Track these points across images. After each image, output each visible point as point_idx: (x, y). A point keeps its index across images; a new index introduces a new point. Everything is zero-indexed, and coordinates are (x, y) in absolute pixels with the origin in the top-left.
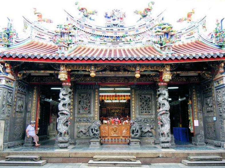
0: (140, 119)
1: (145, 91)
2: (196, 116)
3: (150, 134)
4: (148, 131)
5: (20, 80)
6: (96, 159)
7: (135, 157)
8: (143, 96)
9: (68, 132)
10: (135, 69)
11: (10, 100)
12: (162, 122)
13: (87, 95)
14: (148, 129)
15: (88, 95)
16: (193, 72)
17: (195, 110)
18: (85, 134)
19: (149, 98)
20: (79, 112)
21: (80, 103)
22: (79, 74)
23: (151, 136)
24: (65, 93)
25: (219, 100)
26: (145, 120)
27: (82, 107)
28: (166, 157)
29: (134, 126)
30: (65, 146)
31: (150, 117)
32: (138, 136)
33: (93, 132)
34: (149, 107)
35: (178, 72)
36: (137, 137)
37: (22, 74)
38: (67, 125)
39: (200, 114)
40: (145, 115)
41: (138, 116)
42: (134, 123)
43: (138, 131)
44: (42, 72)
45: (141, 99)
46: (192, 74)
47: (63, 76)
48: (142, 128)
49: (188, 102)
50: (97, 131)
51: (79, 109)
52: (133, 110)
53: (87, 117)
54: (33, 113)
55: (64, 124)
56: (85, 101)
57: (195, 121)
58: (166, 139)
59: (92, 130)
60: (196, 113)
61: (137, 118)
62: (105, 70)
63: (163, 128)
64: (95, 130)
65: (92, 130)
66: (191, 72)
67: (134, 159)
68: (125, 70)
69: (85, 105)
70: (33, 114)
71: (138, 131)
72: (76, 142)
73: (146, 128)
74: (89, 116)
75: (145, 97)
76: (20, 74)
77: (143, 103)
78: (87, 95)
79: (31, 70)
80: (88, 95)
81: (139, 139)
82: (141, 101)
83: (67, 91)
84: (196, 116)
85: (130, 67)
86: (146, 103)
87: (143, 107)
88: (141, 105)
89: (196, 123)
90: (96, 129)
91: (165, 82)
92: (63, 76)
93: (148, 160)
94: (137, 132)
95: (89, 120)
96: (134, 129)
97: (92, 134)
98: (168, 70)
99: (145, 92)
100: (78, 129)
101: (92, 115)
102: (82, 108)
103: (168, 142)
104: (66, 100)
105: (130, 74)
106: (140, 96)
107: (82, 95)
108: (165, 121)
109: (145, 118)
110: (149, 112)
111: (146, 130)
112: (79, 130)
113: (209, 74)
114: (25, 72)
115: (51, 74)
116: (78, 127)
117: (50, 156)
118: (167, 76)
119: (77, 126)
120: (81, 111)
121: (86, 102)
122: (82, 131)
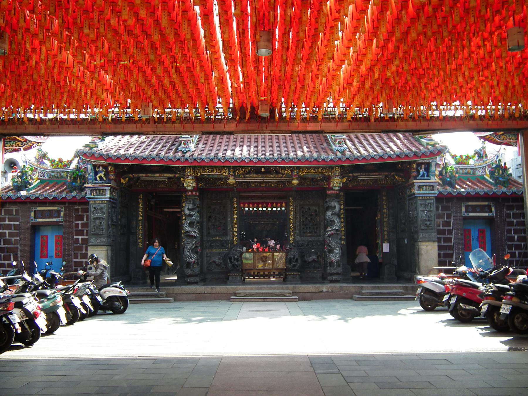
0: (301, 242)
1: (310, 200)
2: (386, 237)
3: (317, 265)
4: (314, 260)
5: (124, 188)
6: (240, 294)
7: (291, 292)
8: (307, 207)
9: (198, 261)
10: (292, 172)
11: (114, 218)
12: (330, 246)
13: (220, 207)
14: (313, 257)
15: (222, 208)
16: (377, 174)
17: (385, 229)
18: (218, 265)
19: (316, 211)
20: (209, 233)
21: (209, 220)
22: (211, 178)
23: (318, 268)
24: (191, 207)
25: (114, 230)
26: (310, 244)
27: (214, 225)
28: (332, 292)
29: (292, 253)
30: (195, 281)
31: (316, 239)
32: (297, 267)
33: (231, 262)
34: (315, 225)
35: (355, 175)
36: (296, 268)
37: (127, 179)
38: (197, 253)
39: (392, 234)
40: (308, 236)
41: (298, 238)
42: (291, 249)
43: (297, 259)
44: (157, 175)
45: (303, 212)
46: (375, 176)
47: (189, 183)
48: (304, 256)
49: (377, 216)
50: (237, 261)
51: (209, 229)
52: (291, 229)
53: (221, 241)
54: (139, 235)
55: (192, 251)
56: (218, 216)
57: (384, 244)
58: (335, 270)
59: (230, 259)
60: (386, 233)
61: (297, 241)
62: (249, 173)
63: (331, 255)
64: (235, 259)
65: (230, 259)
66: (374, 174)
67: (289, 293)
68: (277, 172)
69: (218, 223)
70: (140, 237)
71: (297, 259)
72: (206, 277)
73: (310, 256)
74: (225, 238)
75: (309, 209)
76: (124, 179)
77: (307, 219)
78: (220, 207)
79: (141, 173)
80: (222, 208)
81: (299, 271)
82: (303, 216)
83: (194, 204)
84: (386, 237)
85: (285, 170)
86: (311, 219)
87: (306, 225)
88: (303, 222)
89: (386, 248)
90: (236, 257)
91: (334, 190)
92: (189, 183)
93: (308, 295)
94: (297, 261)
95: (225, 245)
96: (292, 257)
97: (230, 265)
98: (338, 174)
99: (309, 202)
100: (208, 258)
101: (228, 238)
102: (213, 227)
103: (338, 274)
104: (194, 217)
105: (285, 177)
106: (302, 207)
107: (213, 207)
108: (334, 244)
109: (309, 242)
110: (316, 233)
111: (311, 259)
112: (210, 260)
113: (401, 177)
114: (131, 175)
115: (169, 178)
116: (209, 255)
117: (178, 292)
118: (336, 183)
119: (207, 254)
120: (212, 232)
121: (219, 218)
122: (214, 262)
